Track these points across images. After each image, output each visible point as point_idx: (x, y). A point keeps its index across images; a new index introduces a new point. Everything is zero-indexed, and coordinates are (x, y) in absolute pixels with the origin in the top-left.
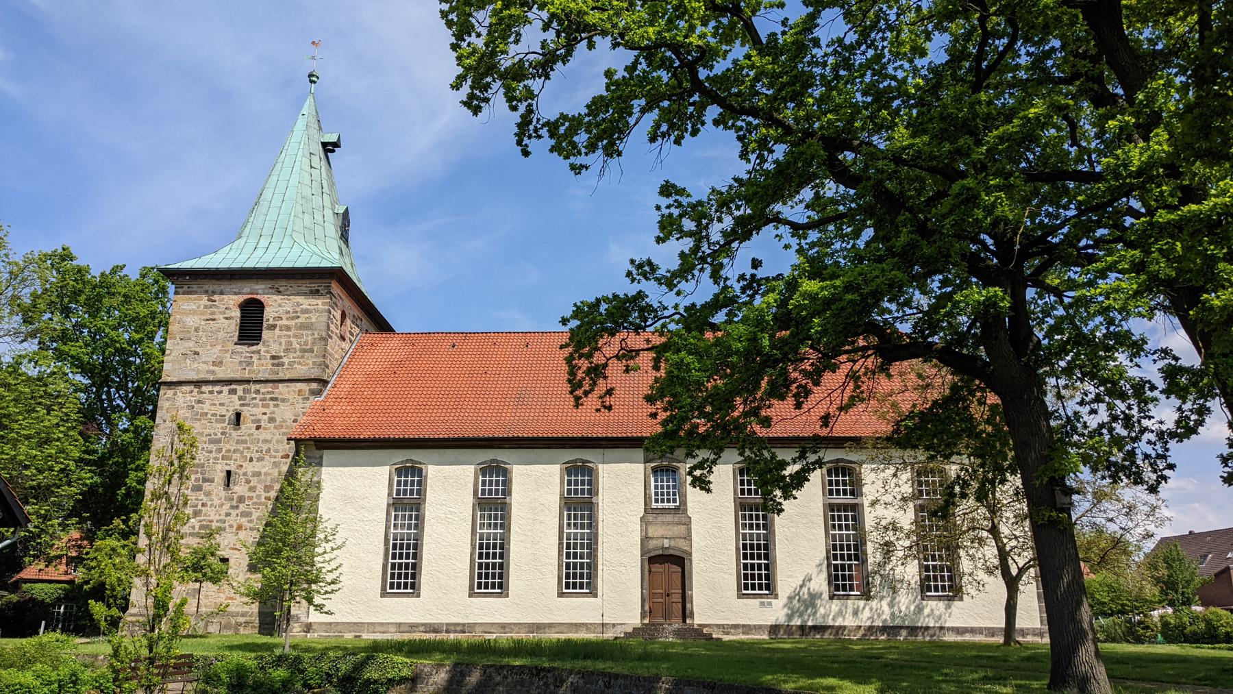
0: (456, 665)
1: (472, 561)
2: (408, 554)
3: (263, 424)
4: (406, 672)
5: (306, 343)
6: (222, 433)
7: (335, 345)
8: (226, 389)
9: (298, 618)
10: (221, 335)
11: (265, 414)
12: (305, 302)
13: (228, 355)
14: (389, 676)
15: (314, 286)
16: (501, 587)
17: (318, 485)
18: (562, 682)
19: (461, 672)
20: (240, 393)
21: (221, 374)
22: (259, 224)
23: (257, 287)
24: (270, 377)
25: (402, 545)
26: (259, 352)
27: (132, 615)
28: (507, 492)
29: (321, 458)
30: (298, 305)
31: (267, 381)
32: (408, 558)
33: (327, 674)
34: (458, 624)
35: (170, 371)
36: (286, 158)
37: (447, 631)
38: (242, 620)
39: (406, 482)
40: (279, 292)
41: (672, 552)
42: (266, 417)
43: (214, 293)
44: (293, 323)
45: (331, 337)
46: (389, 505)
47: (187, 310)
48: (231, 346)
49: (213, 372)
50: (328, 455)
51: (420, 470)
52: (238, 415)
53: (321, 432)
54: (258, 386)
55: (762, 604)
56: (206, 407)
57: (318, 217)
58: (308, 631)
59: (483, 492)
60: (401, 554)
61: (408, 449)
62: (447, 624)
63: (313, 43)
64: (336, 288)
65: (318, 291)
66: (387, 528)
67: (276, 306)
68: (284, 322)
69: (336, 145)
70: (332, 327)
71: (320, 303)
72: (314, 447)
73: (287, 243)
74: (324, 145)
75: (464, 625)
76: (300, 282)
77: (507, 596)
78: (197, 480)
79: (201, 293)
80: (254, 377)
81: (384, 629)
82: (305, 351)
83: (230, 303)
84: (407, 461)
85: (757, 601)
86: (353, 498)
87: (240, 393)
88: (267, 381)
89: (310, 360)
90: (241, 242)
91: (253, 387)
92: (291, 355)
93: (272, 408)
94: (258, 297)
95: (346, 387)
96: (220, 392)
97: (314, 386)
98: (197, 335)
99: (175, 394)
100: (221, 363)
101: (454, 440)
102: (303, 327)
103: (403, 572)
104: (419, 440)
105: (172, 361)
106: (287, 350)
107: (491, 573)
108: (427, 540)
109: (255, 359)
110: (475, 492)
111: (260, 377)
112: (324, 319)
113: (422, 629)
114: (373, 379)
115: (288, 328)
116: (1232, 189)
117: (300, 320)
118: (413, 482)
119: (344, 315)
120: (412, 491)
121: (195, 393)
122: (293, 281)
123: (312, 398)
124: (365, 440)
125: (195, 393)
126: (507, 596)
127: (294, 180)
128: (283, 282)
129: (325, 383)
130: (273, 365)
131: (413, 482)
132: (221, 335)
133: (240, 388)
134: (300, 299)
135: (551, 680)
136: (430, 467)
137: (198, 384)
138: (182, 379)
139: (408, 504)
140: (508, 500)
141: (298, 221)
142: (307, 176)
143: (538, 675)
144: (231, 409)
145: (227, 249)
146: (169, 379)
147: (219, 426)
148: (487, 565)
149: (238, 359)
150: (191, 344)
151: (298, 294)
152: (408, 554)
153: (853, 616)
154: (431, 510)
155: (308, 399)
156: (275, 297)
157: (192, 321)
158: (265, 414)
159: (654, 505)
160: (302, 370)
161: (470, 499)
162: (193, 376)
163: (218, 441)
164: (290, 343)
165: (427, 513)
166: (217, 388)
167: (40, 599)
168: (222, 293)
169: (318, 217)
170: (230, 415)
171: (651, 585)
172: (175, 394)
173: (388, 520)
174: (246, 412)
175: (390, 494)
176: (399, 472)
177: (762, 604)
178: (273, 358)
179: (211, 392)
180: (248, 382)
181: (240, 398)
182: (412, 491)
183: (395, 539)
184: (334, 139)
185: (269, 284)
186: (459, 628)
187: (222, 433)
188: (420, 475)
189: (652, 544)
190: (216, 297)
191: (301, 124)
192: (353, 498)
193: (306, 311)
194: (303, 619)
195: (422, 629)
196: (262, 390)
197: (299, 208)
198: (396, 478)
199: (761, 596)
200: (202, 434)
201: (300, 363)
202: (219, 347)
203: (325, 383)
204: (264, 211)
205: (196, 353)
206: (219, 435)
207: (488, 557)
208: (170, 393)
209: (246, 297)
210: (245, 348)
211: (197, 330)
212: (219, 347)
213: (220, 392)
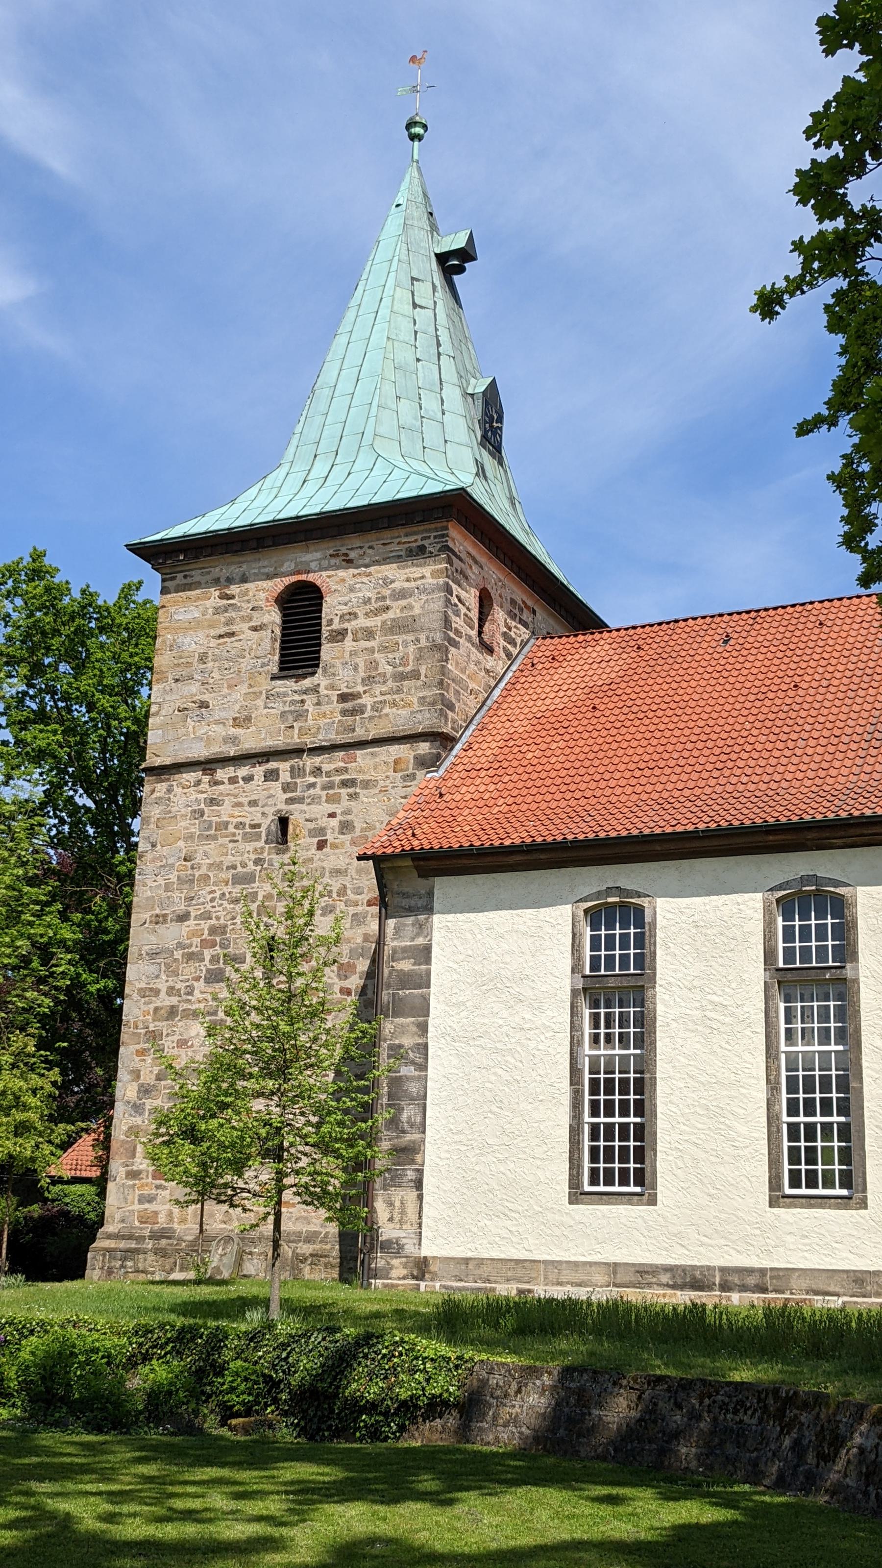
0: (567, 1372)
1: (772, 1119)
2: (624, 1104)
3: (329, 837)
4: (444, 1385)
5: (404, 661)
6: (257, 862)
7: (465, 659)
8: (259, 771)
9: (401, 1247)
10: (246, 664)
11: (332, 815)
12: (399, 575)
13: (260, 702)
14: (404, 1395)
15: (415, 540)
16: (851, 1184)
17: (425, 954)
18: (839, 1442)
19: (581, 1393)
20: (285, 776)
21: (251, 742)
22: (312, 433)
23: (308, 557)
24: (341, 739)
25: (609, 1082)
26: (315, 689)
27: (109, 1237)
28: (847, 952)
29: (430, 894)
30: (387, 582)
31: (334, 748)
32: (624, 1113)
33: (268, 1379)
34: (750, 1271)
35: (160, 746)
36: (365, 296)
37: (725, 1287)
38: (306, 1249)
39: (610, 939)
40: (349, 562)
42: (334, 823)
43: (230, 581)
44: (377, 621)
45: (456, 645)
46: (574, 993)
47: (189, 622)
48: (265, 684)
50: (444, 887)
51: (640, 911)
52: (284, 822)
53: (431, 837)
54: (317, 760)
56: (226, 812)
57: (431, 404)
58: (420, 1277)
59: (789, 954)
60: (609, 1104)
61: (607, 864)
62: (723, 1270)
63: (413, 59)
64: (459, 539)
65: (422, 549)
66: (575, 1044)
67: (347, 590)
68: (362, 622)
69: (466, 255)
70: (458, 622)
71: (427, 573)
72: (411, 875)
73: (364, 460)
74: (442, 258)
75: (763, 1272)
76: (387, 534)
77: (863, 1204)
78: (214, 959)
79: (208, 585)
80: (310, 741)
81: (579, 1277)
82: (401, 677)
83: (259, 598)
84: (609, 891)
86: (499, 976)
87: (285, 776)
88: (334, 748)
89: (414, 693)
90: (281, 472)
91: (309, 762)
92: (378, 689)
93: (345, 803)
94: (311, 577)
95: (491, 747)
96: (248, 779)
97: (424, 748)
98: (208, 668)
99: (170, 790)
100: (248, 719)
101: (708, 834)
102: (397, 627)
103: (616, 1144)
104: (630, 840)
105: (160, 727)
106: (368, 680)
108: (663, 1069)
109: (309, 705)
110: (769, 956)
111: (322, 739)
112: (437, 604)
113: (665, 1278)
114: (550, 725)
115: (369, 634)
117: (391, 615)
118: (624, 938)
119: (485, 601)
120: (624, 959)
121: (204, 786)
122: (373, 535)
123: (420, 774)
124: (514, 850)
125: (204, 786)
126: (863, 1204)
127: (378, 337)
128: (355, 541)
129: (446, 741)
130: (344, 713)
131: (624, 938)
132: (246, 664)
133: (283, 767)
134: (390, 570)
135: (810, 1436)
136: (660, 902)
137: (208, 765)
138: (181, 758)
139: (616, 990)
140: (849, 972)
141: (386, 414)
142: (406, 326)
143: (780, 1415)
144: (270, 810)
145: (254, 491)
146: (158, 762)
147: (250, 846)
148: (810, 1130)
149: (279, 707)
150: (193, 688)
151: (385, 561)
152: (624, 1104)
154: (668, 1002)
155: (413, 777)
156: (341, 573)
157: (193, 643)
158: (332, 815)
160: (401, 717)
161: (756, 975)
162: (200, 752)
163: (249, 879)
164: (373, 665)
165: (660, 1009)
166: (243, 771)
167: (75, 1211)
168: (244, 580)
169: (431, 404)
170: (268, 823)
172: (170, 790)
173: (575, 1027)
174: (298, 816)
175: (576, 968)
176: (594, 917)
178: (344, 698)
179: (233, 780)
180: (298, 752)
181: (286, 788)
182: (624, 959)
183: (594, 1070)
184: (459, 242)
185: (328, 547)
186: (751, 1281)
187: (257, 862)
188: (640, 923)
190: (234, 589)
191: (394, 223)
192: (499, 976)
193: (402, 594)
194: (410, 1248)
195: (665, 1278)
196: (326, 767)
197: (389, 389)
198: (588, 932)
200: (218, 866)
201: (394, 704)
202: (243, 689)
203: (446, 741)
204: (323, 408)
205: (204, 705)
206: (251, 866)
207: (810, 1110)
208: (161, 788)
209: (288, 580)
210: (290, 684)
211: (203, 659)
212: (243, 689)
213: (248, 779)
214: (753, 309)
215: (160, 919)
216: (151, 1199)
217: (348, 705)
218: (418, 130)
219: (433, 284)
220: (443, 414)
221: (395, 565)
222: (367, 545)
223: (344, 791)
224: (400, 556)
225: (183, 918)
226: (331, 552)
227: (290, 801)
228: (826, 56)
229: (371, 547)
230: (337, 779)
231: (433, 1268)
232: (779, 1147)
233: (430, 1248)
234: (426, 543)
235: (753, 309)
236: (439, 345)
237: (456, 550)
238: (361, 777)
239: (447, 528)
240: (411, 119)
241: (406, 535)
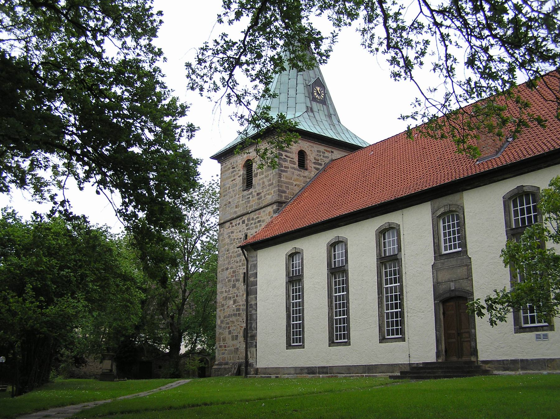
5: (270, 180)
41: (457, 294)
49: (235, 212)
52: (246, 235)
55: (538, 337)
57: (292, 92)
62: (319, 367)
80: (249, 210)
85: (533, 335)
92: (265, 190)
97: (275, 207)
106: (263, 187)
107: (339, 332)
116: (62, 3)
144: (243, 233)
153: (340, 357)
159: (444, 252)
169: (292, 92)
171: (447, 327)
177: (538, 337)
181: (247, 225)
189: (443, 287)
194: (255, 365)
196: (255, 217)
199: (536, 329)
215: (223, 270)
216: (223, 354)
217: (259, 196)
223: (258, 224)
225: (227, 269)
227: (247, 229)
228: (239, 20)
230: (257, 220)
231: (259, 371)
232: (383, 321)
233: (259, 366)
238: (262, 219)
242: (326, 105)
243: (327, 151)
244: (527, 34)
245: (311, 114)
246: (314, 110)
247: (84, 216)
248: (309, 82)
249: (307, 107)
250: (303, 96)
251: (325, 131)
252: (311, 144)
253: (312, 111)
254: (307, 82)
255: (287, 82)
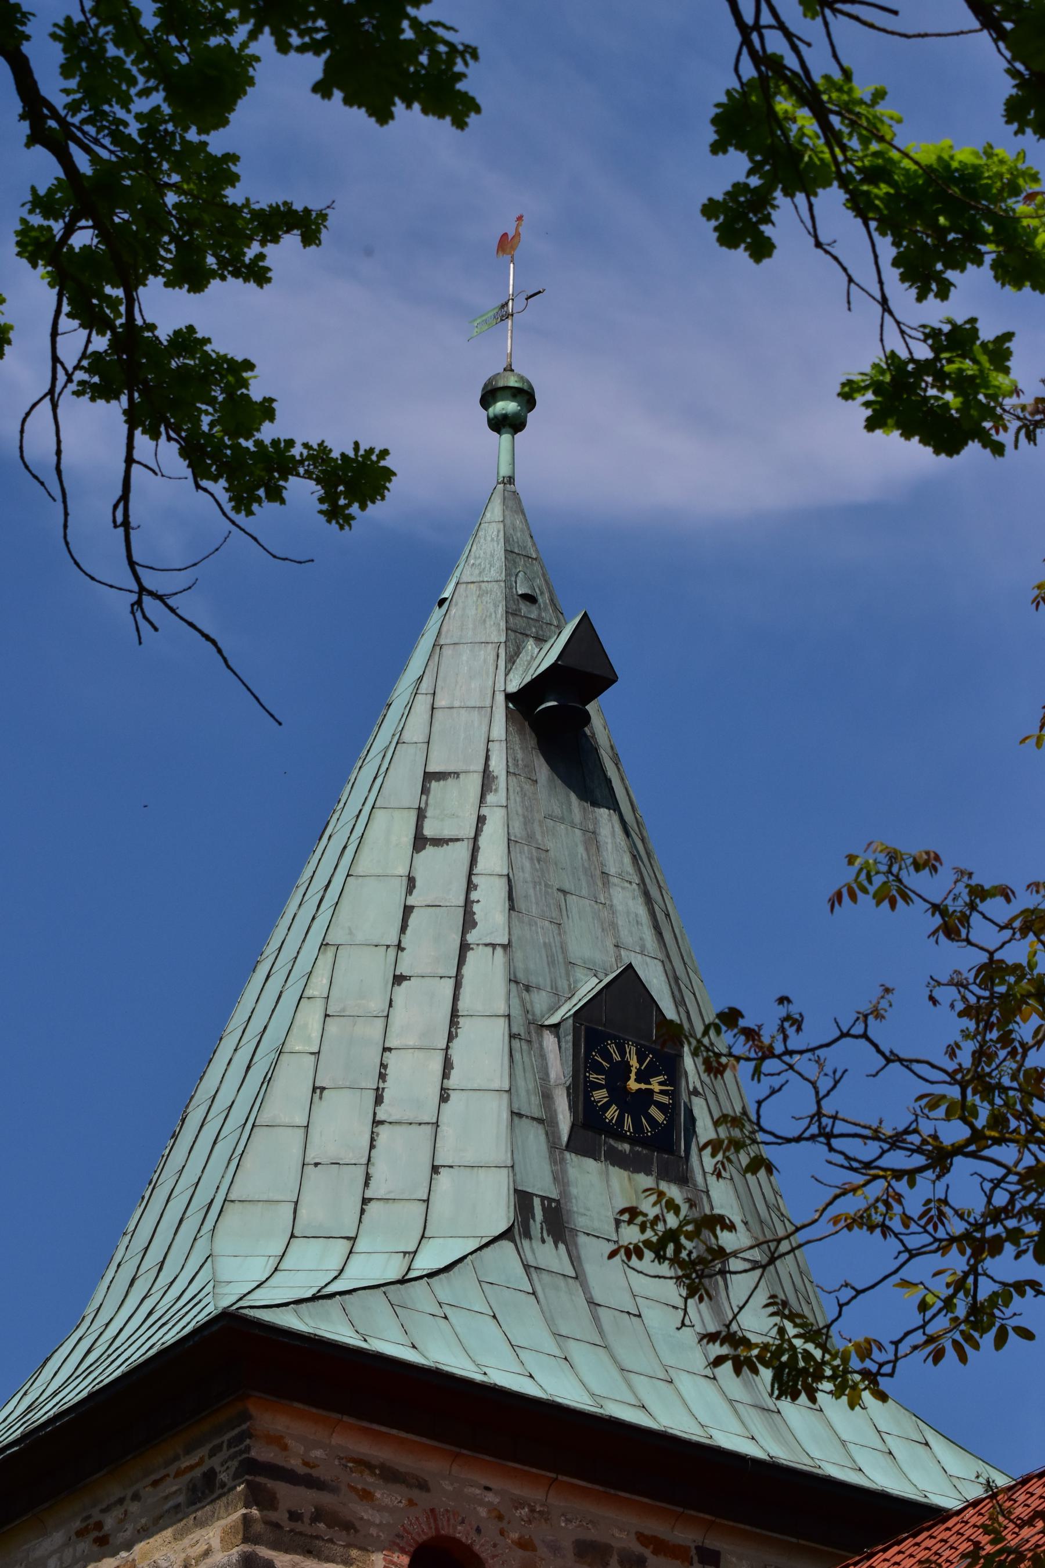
57: (413, 1079)
169: (413, 1079)
214: (710, 209)
218: (506, 406)
219: (486, 773)
220: (444, 1097)
221: (168, 1533)
222: (130, 1493)
224: (177, 1507)
226: (77, 1524)
229: (136, 1497)
234: (215, 1462)
235: (710, 209)
236: (469, 922)
237: (295, 1463)
239: (246, 1416)
240: (490, 381)
241: (188, 1451)
242: (613, 805)
243: (660, 1546)
244: (439, 53)
245: (549, 1255)
246: (581, 1222)
247: (265, 398)
248: (558, 999)
249: (523, 1200)
250: (496, 1109)
251: (647, 1391)
252: (534, 1494)
253: (558, 1224)
254: (540, 1001)
255: (377, 1004)
